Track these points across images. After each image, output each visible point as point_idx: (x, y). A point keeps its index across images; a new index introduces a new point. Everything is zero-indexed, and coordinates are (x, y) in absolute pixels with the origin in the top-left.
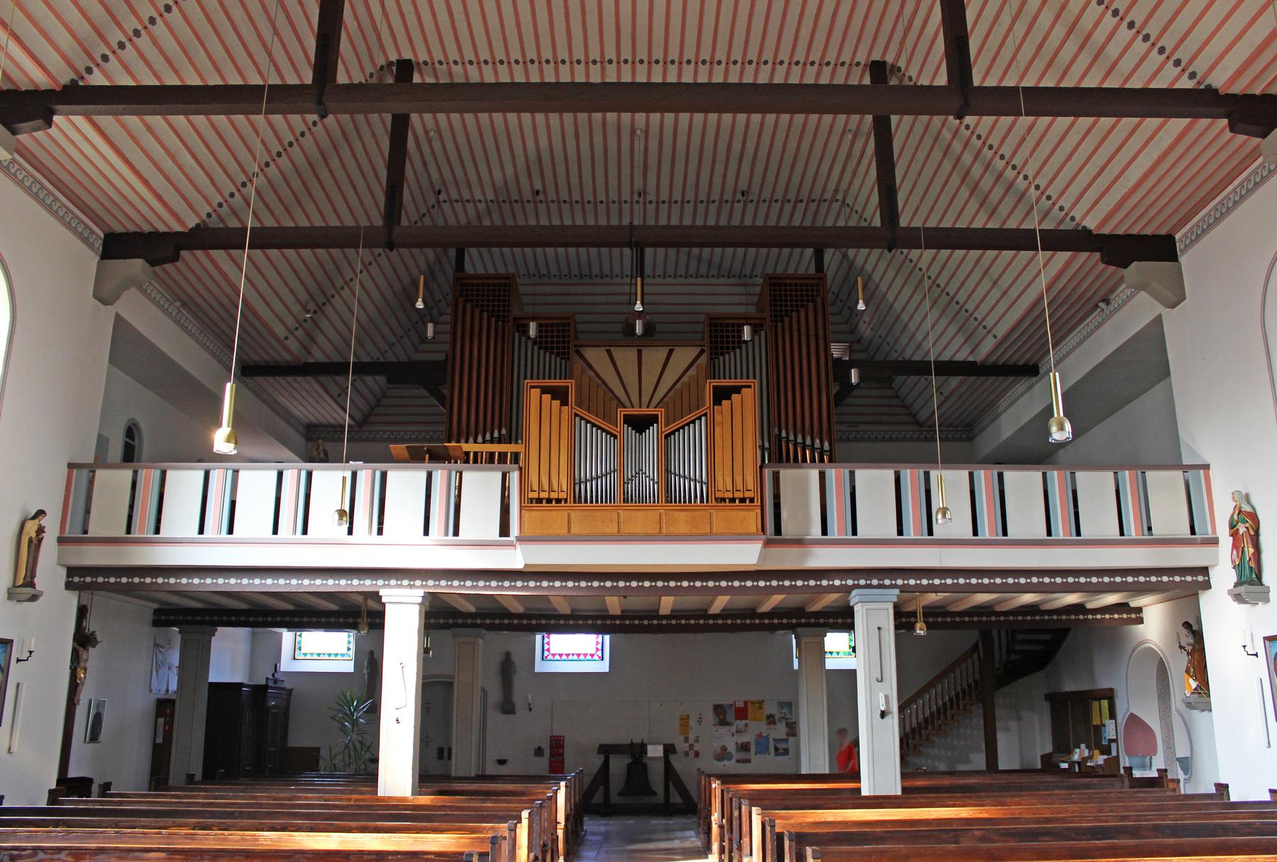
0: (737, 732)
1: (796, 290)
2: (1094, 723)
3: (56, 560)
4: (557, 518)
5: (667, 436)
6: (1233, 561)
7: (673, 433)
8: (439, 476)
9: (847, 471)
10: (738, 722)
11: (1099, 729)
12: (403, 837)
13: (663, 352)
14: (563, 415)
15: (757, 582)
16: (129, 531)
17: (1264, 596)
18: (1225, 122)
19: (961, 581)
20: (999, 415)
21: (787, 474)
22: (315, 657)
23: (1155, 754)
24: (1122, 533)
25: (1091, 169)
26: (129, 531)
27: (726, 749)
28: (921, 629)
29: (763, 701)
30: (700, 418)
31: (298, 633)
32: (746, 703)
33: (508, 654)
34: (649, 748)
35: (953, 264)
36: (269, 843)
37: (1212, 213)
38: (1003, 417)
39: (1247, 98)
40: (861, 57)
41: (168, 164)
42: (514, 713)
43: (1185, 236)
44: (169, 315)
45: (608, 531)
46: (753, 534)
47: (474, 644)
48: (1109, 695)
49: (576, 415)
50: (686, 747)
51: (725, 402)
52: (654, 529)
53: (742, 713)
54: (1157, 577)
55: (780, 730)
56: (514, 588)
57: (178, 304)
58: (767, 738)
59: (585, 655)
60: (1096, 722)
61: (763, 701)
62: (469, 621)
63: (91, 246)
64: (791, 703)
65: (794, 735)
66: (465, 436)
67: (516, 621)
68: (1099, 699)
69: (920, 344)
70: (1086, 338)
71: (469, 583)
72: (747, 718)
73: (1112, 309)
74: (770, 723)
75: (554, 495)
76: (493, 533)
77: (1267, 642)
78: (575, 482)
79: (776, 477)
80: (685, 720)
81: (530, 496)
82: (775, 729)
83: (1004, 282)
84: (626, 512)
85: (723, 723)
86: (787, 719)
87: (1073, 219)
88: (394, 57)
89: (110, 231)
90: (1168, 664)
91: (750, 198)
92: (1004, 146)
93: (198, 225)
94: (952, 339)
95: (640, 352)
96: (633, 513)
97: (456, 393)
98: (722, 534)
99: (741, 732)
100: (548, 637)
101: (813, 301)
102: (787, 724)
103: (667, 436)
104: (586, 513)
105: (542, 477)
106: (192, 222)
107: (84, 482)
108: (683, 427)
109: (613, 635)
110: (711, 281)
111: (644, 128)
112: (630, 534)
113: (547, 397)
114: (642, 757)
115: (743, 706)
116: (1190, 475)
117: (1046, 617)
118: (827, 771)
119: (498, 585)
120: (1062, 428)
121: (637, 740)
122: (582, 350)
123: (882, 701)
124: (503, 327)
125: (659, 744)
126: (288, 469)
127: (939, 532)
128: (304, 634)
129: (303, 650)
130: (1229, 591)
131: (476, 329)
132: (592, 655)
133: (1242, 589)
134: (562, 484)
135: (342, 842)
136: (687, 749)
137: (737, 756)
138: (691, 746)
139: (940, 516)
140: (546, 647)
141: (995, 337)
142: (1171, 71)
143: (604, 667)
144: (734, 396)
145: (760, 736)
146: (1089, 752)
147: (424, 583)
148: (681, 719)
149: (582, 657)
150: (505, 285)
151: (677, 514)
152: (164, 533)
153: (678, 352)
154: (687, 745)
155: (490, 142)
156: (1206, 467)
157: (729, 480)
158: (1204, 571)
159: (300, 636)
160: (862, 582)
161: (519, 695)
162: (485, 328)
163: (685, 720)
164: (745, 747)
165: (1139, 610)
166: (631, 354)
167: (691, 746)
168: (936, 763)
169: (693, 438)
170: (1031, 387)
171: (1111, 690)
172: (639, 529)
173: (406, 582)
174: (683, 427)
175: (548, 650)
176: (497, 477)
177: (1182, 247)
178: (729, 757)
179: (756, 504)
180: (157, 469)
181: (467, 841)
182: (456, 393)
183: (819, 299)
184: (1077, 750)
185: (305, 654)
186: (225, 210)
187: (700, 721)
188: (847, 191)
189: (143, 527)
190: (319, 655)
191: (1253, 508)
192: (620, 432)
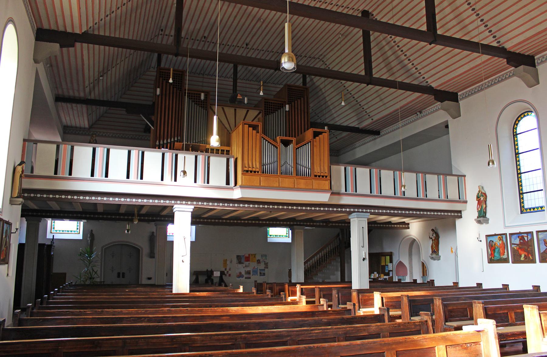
0: (246, 266)
2: (382, 264)
4: (255, 179)
5: (297, 149)
6: (478, 209)
7: (298, 148)
8: (201, 158)
9: (354, 168)
10: (246, 262)
11: (384, 267)
12: (286, 307)
13: (245, 111)
14: (257, 137)
16: (56, 173)
17: (487, 221)
18: (505, 60)
19: (400, 212)
20: (355, 148)
21: (334, 167)
22: (61, 232)
23: (407, 276)
24: (371, 193)
25: (443, 66)
26: (56, 173)
27: (241, 273)
30: (308, 143)
31: (53, 221)
32: (249, 255)
34: (215, 272)
36: (234, 312)
37: (481, 86)
38: (358, 149)
39: (514, 54)
40: (361, 8)
43: (463, 94)
45: (275, 185)
48: (391, 255)
49: (262, 137)
52: (291, 186)
53: (248, 259)
54: (238, 204)
55: (262, 266)
56: (229, 206)
60: (383, 264)
62: (122, 217)
65: (267, 268)
66: (162, 138)
68: (385, 256)
69: (335, 118)
70: (409, 123)
71: (211, 204)
72: (249, 261)
73: (423, 115)
74: (258, 263)
75: (254, 170)
76: (224, 184)
77: (487, 237)
78: (262, 165)
80: (225, 261)
81: (244, 169)
83: (386, 101)
84: (282, 179)
85: (240, 262)
86: (265, 262)
87: (427, 82)
89: (40, 27)
90: (420, 244)
91: (208, 40)
92: (408, 52)
94: (352, 117)
95: (235, 110)
96: (284, 179)
97: (159, 119)
98: (317, 189)
103: (297, 149)
105: (249, 162)
108: (302, 146)
109: (197, 225)
110: (252, 82)
111: (264, 19)
112: (283, 187)
114: (211, 277)
116: (460, 178)
117: (379, 225)
119: (191, 204)
121: (209, 270)
122: (211, 106)
123: (364, 255)
124: (179, 93)
125: (218, 271)
126: (98, 147)
128: (56, 222)
129: (56, 229)
130: (475, 220)
131: (168, 92)
133: (480, 219)
134: (257, 166)
135: (285, 309)
137: (245, 276)
141: (372, 119)
142: (491, 39)
143: (80, 237)
146: (379, 275)
147: (192, 203)
148: (224, 261)
151: (300, 180)
152: (74, 175)
155: (197, 13)
156: (465, 176)
157: (319, 168)
158: (460, 212)
159: (54, 222)
160: (356, 210)
162: (171, 92)
163: (225, 261)
164: (248, 273)
165: (408, 224)
166: (232, 110)
169: (306, 150)
170: (375, 139)
171: (391, 253)
172: (286, 185)
173: (184, 202)
174: (302, 146)
176: (224, 160)
177: (461, 98)
178: (242, 276)
180: (70, 145)
181: (308, 307)
182: (159, 119)
183: (305, 97)
184: (373, 274)
185: (56, 231)
187: (231, 262)
188: (325, 56)
189: (63, 171)
190: (63, 231)
191: (485, 192)
192: (279, 146)
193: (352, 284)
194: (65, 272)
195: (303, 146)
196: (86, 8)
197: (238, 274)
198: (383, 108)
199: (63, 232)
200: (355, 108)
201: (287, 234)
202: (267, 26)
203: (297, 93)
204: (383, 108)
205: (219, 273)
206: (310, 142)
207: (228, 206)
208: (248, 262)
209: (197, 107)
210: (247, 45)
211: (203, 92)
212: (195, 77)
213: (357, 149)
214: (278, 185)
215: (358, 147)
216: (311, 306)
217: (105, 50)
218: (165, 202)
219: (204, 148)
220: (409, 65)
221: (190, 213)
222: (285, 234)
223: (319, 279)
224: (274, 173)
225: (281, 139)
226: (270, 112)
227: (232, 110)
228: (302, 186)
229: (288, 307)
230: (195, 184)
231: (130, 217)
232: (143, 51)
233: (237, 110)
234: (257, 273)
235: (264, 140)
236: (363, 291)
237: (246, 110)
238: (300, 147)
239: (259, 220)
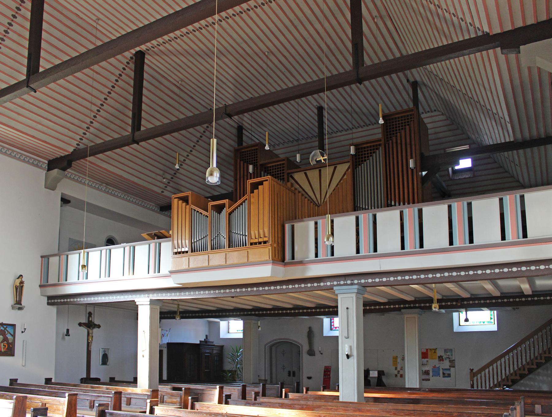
1: (402, 120)
3: (40, 294)
15: (307, 284)
28: (435, 308)
29: (436, 349)
32: (427, 350)
33: (310, 328)
34: (371, 372)
35: (151, 80)
41: (40, 127)
42: (315, 356)
44: (101, 190)
46: (267, 260)
47: (250, 323)
50: (396, 372)
51: (256, 191)
55: (446, 364)
56: (185, 295)
57: (104, 185)
58: (439, 368)
61: (436, 349)
63: (40, 167)
64: (452, 350)
65: (454, 367)
74: (440, 360)
79: (293, 227)
82: (443, 363)
86: (449, 358)
93: (74, 150)
99: (424, 365)
101: (408, 125)
102: (450, 361)
106: (71, 149)
107: (46, 262)
113: (180, 202)
115: (425, 351)
118: (418, 387)
120: (211, 174)
136: (397, 373)
138: (399, 371)
140: (332, 324)
144: (260, 187)
145: (435, 367)
152: (68, 281)
154: (397, 371)
161: (317, 347)
167: (399, 371)
168: (541, 385)
175: (333, 325)
186: (84, 141)
201: (491, 318)
205: (376, 373)
208: (426, 360)
217: (433, 44)
222: (489, 320)
231: (428, 305)
232: (450, 44)
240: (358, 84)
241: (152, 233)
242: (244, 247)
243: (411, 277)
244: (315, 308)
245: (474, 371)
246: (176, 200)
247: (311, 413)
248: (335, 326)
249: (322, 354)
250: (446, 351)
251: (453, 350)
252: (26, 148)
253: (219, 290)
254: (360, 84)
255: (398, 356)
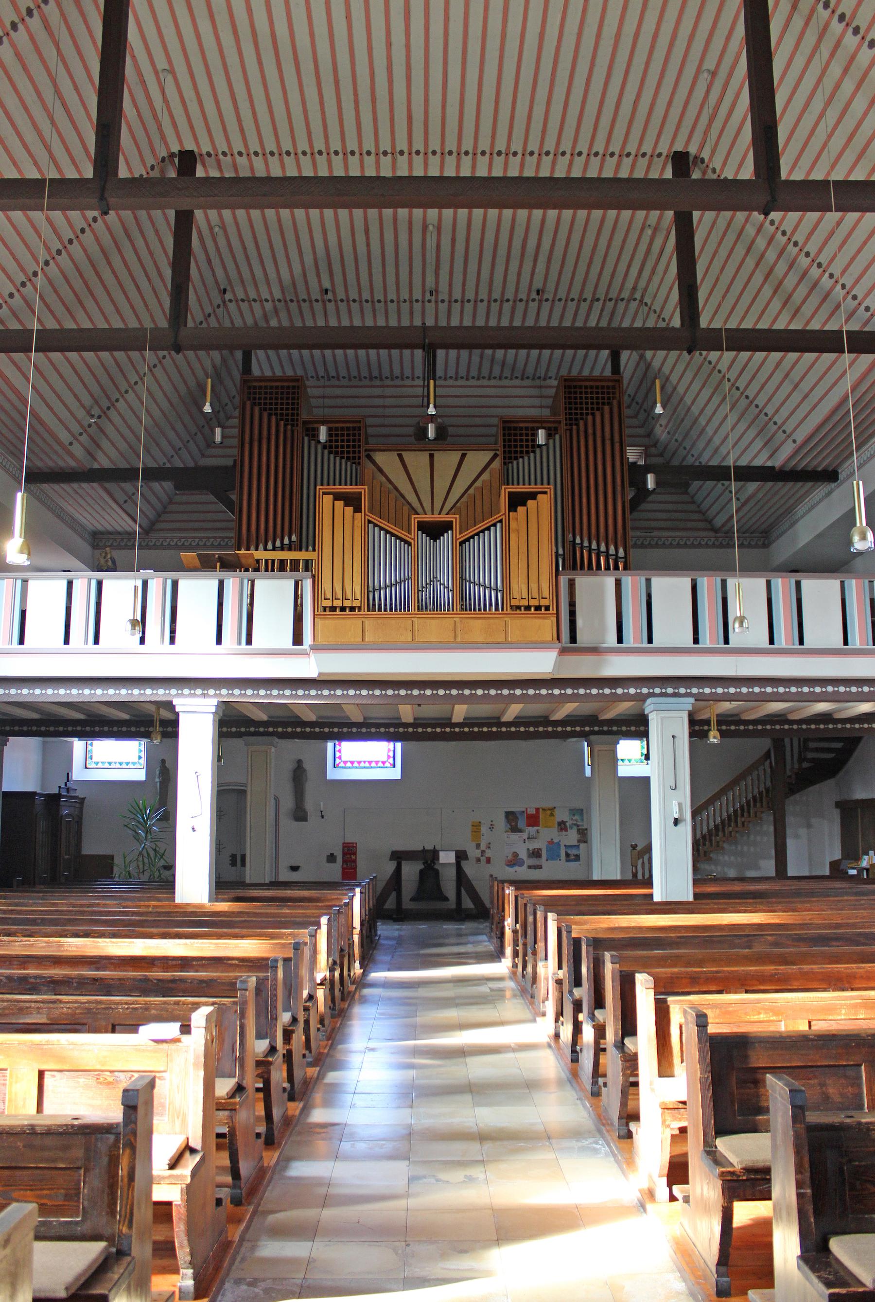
4: (350, 625)
7: (468, 540)
8: (232, 583)
9: (719, 580)
10: (530, 828)
13: (456, 456)
14: (356, 522)
22: (107, 765)
28: (714, 737)
31: (89, 742)
32: (537, 810)
33: (299, 762)
34: (441, 854)
36: (75, 949)
40: (664, 148)
45: (402, 639)
49: (369, 522)
50: (478, 853)
51: (521, 509)
52: (448, 637)
53: (533, 820)
56: (309, 696)
58: (558, 844)
59: (377, 763)
62: (261, 729)
64: (582, 810)
65: (586, 842)
67: (308, 730)
72: (538, 825)
74: (561, 830)
75: (347, 603)
78: (369, 590)
79: (572, 584)
80: (476, 827)
83: (805, 386)
84: (421, 621)
85: (515, 829)
86: (578, 826)
88: (175, 148)
95: (432, 456)
96: (428, 621)
97: (245, 497)
100: (340, 745)
101: (608, 404)
102: (578, 830)
104: (380, 621)
112: (425, 643)
113: (339, 504)
114: (434, 863)
120: (864, 538)
121: (429, 847)
122: (371, 453)
123: (676, 809)
124: (292, 432)
127: (657, 641)
129: (94, 759)
132: (384, 763)
134: (355, 592)
136: (479, 855)
138: (483, 852)
139: (737, 625)
140: (338, 754)
143: (140, 775)
144: (530, 503)
145: (551, 842)
149: (373, 765)
150: (294, 387)
153: (470, 455)
154: (479, 851)
159: (92, 745)
160: (657, 691)
163: (476, 827)
164: (536, 854)
167: (483, 852)
175: (340, 757)
179: (551, 611)
182: (245, 497)
183: (615, 402)
184: (866, 857)
185: (97, 763)
187: (491, 828)
190: (110, 763)
192: (414, 539)
193: (174, 893)
194: (111, 854)
195: (481, 535)
196: (608, 247)
197: (510, 857)
198: (806, 407)
199: (110, 766)
200: (749, 417)
202: (453, 240)
203: (584, 396)
204: (806, 407)
206: (501, 521)
207: (304, 697)
208: (536, 828)
209: (335, 460)
210: (538, 292)
211: (323, 423)
212: (361, 387)
213: (800, 525)
214: (410, 639)
215: (802, 517)
216: (273, 944)
218: (155, 692)
219: (251, 561)
220: (823, 279)
221: (211, 716)
223: (726, 870)
224: (400, 606)
225: (418, 522)
226: (516, 452)
227: (424, 457)
228: (477, 637)
229: (211, 943)
230: (219, 646)
233: (437, 455)
234: (559, 856)
235: (376, 529)
236: (673, 906)
237: (460, 453)
238: (478, 534)
239: (500, 724)
240: (173, 353)
241: (215, 555)
242: (451, 612)
243: (775, 690)
244: (414, 725)
245: (639, 848)
246: (328, 499)
247: (261, 944)
248: (344, 759)
249: (323, 817)
250: (574, 811)
251: (585, 811)
252: (568, 438)
253: (153, 690)
254: (178, 352)
255: (483, 822)
